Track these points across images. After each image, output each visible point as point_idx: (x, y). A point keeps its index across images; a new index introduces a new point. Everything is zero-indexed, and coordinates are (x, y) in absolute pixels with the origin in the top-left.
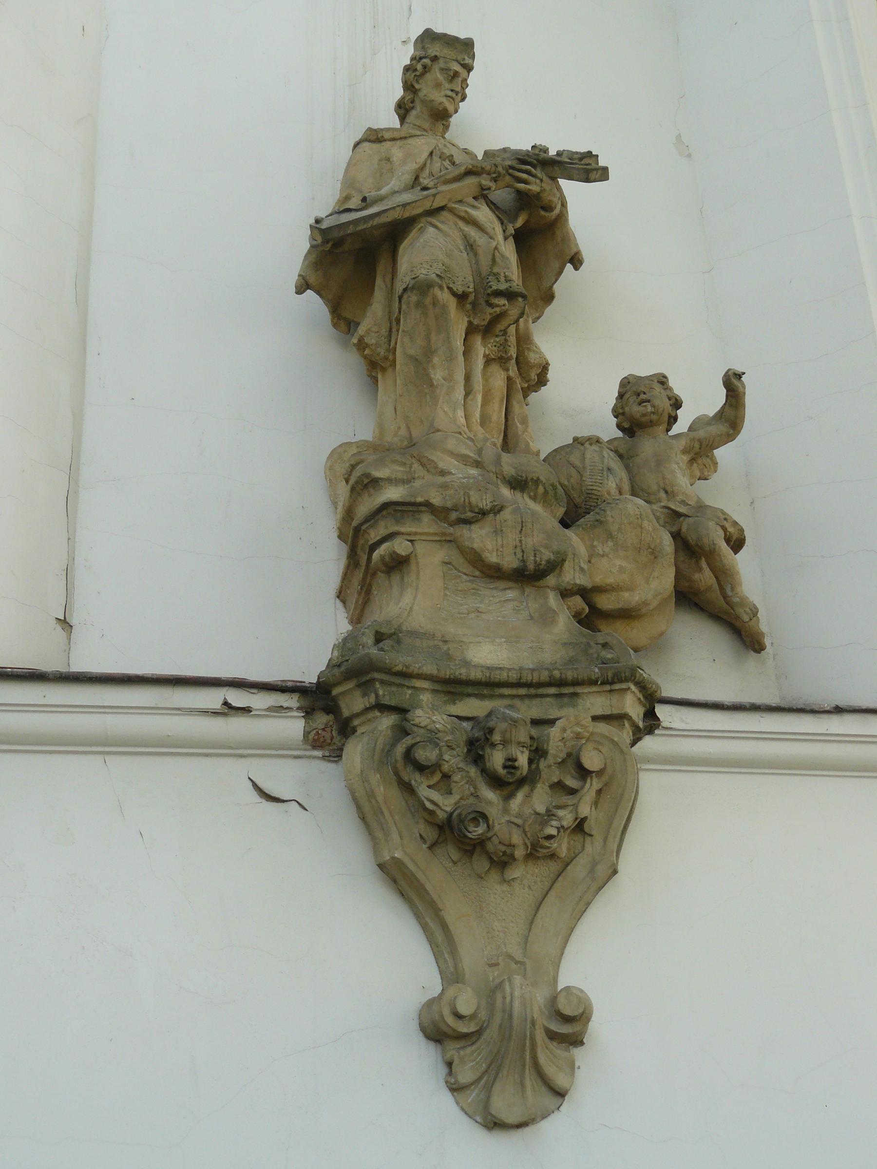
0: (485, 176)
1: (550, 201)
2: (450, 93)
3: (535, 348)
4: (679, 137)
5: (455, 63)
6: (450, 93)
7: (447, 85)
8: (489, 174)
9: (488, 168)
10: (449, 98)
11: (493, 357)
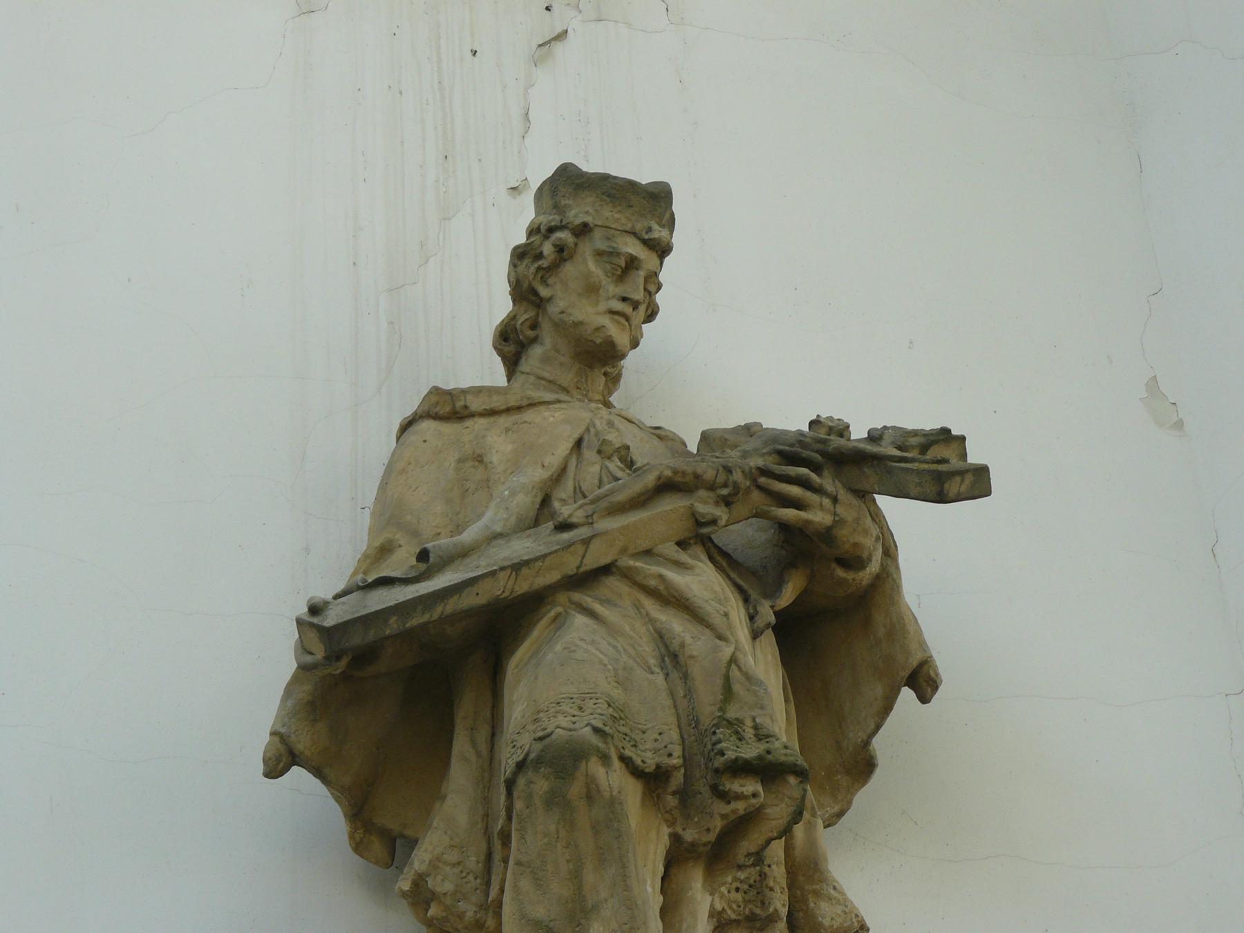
0: (702, 493)
1: (856, 545)
2: (618, 306)
3: (832, 892)
4: (1153, 385)
5: (630, 240)
6: (618, 306)
7: (613, 289)
8: (712, 487)
9: (709, 475)
10: (616, 317)
11: (733, 916)
